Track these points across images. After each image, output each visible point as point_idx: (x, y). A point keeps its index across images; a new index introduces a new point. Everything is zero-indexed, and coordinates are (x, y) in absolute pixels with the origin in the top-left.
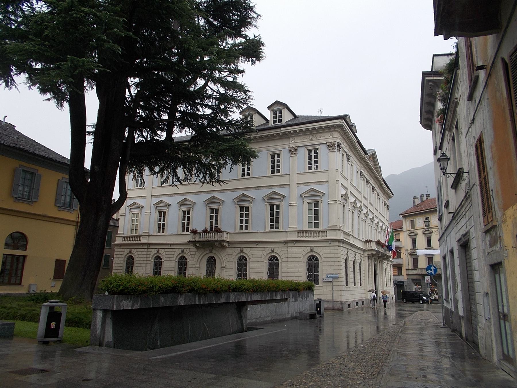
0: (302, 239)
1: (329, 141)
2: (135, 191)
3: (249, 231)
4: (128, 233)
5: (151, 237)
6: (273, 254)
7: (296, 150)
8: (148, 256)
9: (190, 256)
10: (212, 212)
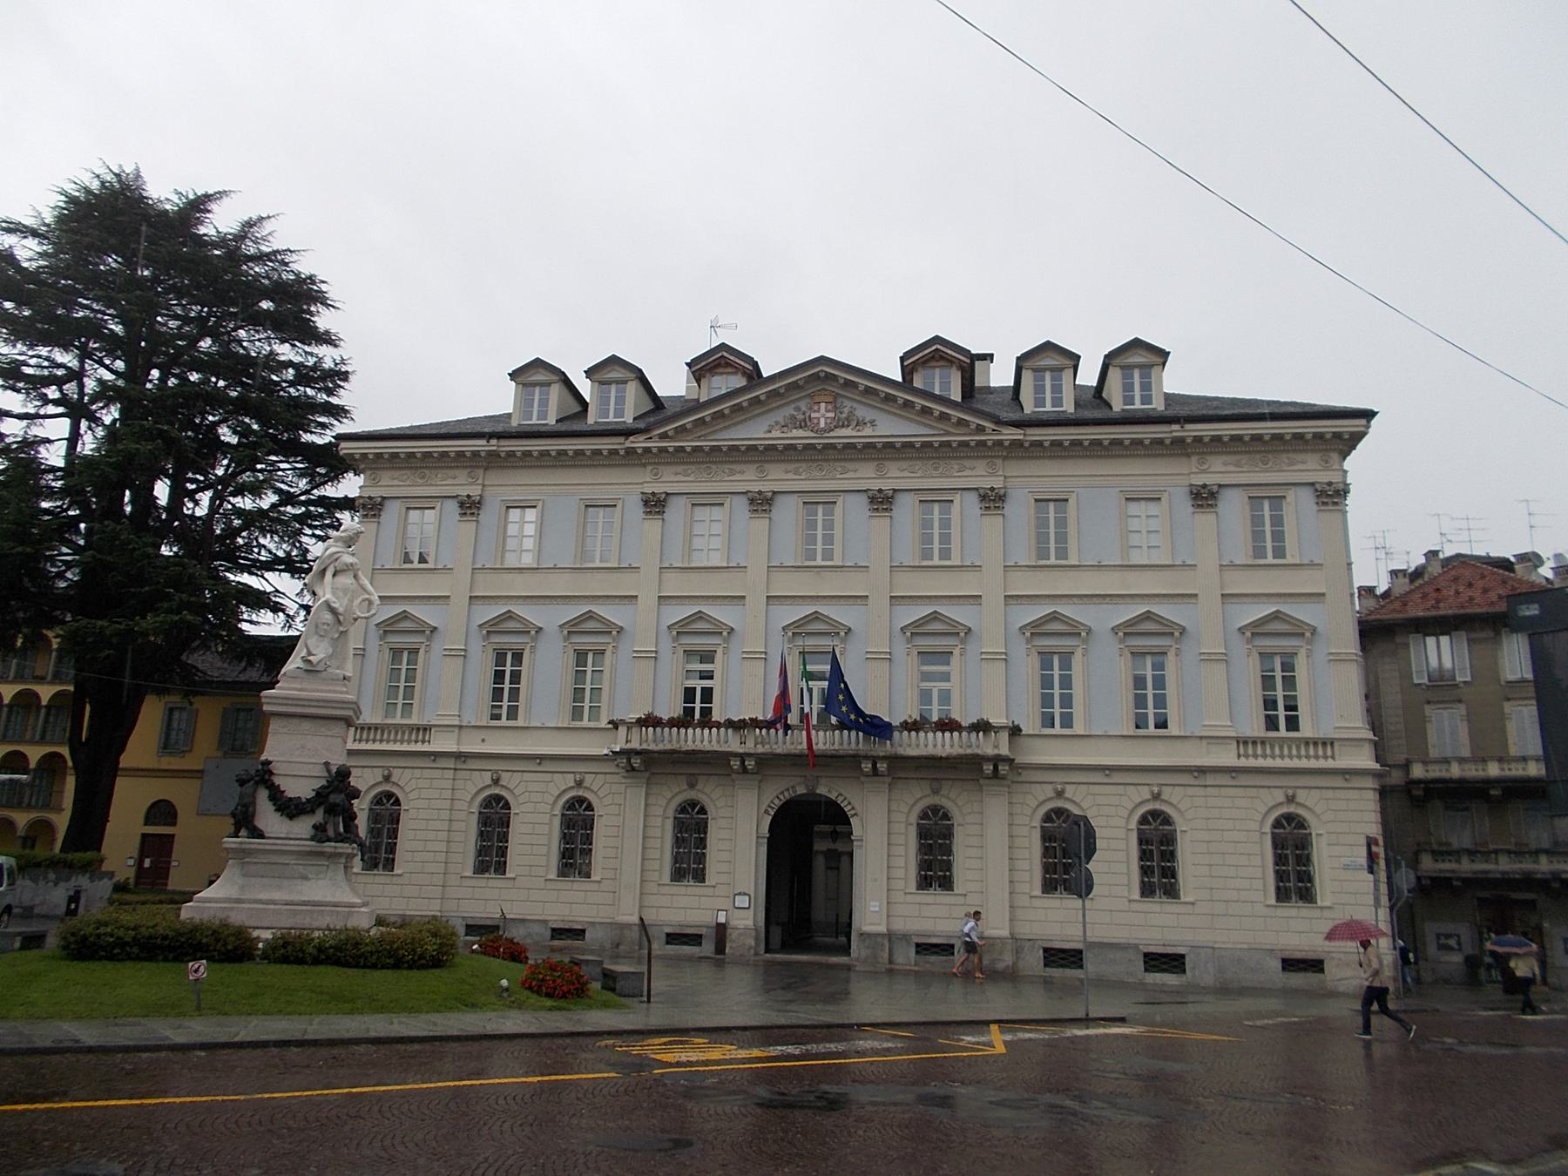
2: (1040, 575)
3: (520, 722)
5: (464, 731)
6: (497, 791)
7: (1213, 495)
8: (458, 795)
9: (607, 801)
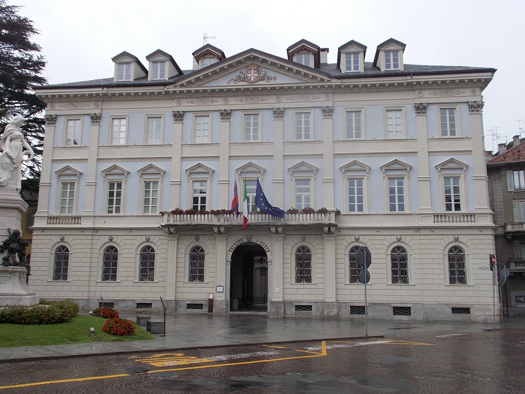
0: (440, 224)
1: (276, 106)
2: (444, 142)
3: (121, 214)
4: (55, 213)
5: (96, 219)
7: (425, 108)
10: (351, 184)
